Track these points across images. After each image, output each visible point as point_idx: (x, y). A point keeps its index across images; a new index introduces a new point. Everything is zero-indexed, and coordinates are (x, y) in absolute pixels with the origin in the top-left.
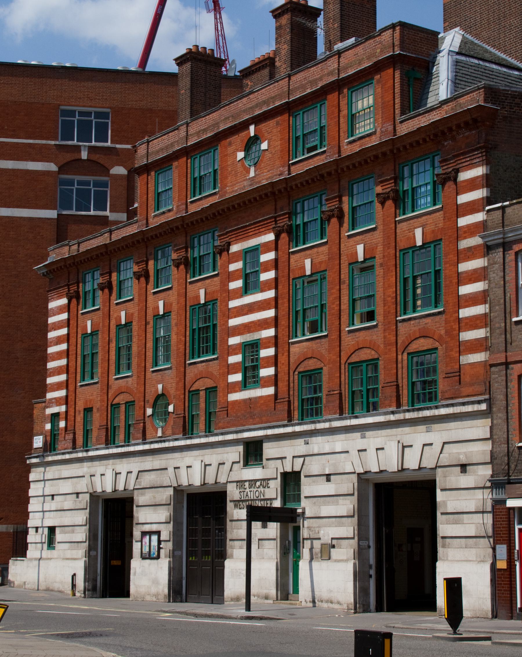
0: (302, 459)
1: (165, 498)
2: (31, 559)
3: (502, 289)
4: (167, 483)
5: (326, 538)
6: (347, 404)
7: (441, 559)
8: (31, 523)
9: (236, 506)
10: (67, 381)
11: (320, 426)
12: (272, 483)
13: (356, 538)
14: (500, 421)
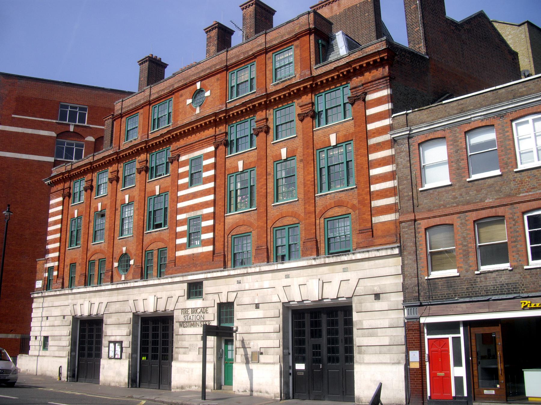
0: (235, 294)
1: (126, 319)
2: (32, 356)
3: (409, 169)
4: (128, 309)
5: (255, 347)
6: (272, 255)
7: (357, 362)
8: (32, 334)
9: (181, 325)
10: (60, 247)
11: (250, 270)
12: (210, 310)
13: (281, 348)
14: (410, 262)
